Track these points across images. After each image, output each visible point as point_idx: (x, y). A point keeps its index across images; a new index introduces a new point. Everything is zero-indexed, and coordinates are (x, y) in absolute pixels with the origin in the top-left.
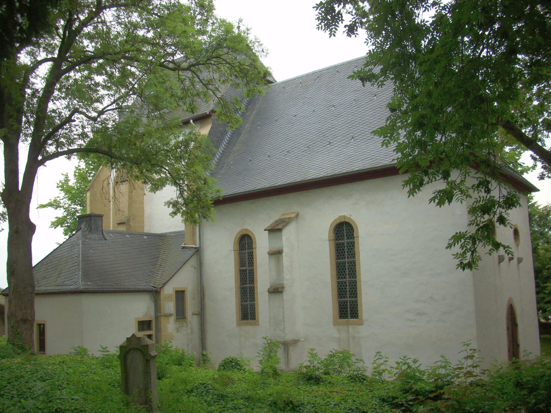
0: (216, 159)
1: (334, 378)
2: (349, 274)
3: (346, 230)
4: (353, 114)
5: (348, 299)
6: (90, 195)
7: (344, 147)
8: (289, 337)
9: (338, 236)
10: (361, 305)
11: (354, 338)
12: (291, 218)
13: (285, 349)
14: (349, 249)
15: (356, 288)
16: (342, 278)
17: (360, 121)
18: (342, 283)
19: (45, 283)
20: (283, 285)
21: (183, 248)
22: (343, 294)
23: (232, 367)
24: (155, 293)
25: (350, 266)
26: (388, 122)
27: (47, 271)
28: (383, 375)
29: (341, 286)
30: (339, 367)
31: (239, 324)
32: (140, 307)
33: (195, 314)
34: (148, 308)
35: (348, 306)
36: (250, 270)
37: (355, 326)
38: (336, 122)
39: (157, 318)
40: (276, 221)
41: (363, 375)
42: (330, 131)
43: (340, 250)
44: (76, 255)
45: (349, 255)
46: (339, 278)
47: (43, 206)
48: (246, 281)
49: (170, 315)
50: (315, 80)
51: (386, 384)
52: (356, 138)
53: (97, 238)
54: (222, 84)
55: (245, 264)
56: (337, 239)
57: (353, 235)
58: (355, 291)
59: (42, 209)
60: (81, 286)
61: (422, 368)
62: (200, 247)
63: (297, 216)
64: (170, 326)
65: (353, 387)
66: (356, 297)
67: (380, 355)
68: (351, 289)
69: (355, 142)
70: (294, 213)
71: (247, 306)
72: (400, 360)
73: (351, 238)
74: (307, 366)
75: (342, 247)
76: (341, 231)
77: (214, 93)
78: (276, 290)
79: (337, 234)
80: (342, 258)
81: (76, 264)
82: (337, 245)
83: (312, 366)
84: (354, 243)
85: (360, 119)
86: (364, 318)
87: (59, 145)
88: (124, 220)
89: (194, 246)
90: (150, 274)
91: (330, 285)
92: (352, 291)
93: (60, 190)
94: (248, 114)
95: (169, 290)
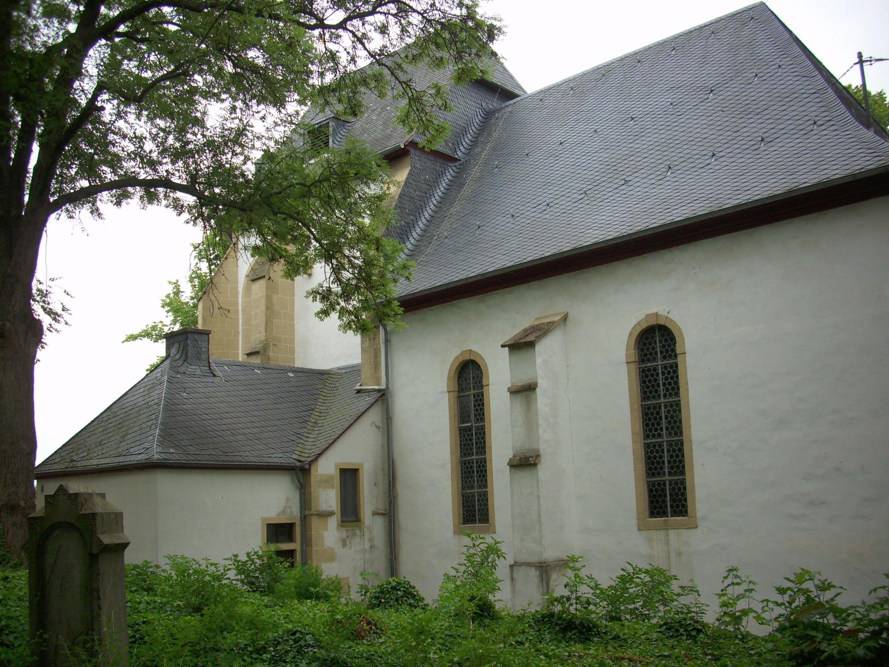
0: (418, 231)
1: (628, 627)
2: (667, 429)
3: (661, 341)
4: (669, 128)
5: (667, 478)
6: (203, 307)
7: (654, 186)
8: (550, 554)
9: (645, 355)
10: (693, 488)
11: (679, 554)
12: (553, 322)
13: (541, 577)
14: (666, 378)
15: (683, 456)
16: (654, 436)
17: (684, 138)
18: (654, 446)
19: (100, 453)
20: (538, 450)
21: (359, 391)
22: (656, 469)
23: (397, 600)
24: (300, 472)
25: (669, 412)
27: (105, 432)
28: (744, 623)
29: (652, 452)
30: (643, 606)
31: (458, 532)
32: (273, 498)
33: (378, 514)
34: (288, 500)
35: (666, 491)
36: (477, 428)
38: (638, 146)
39: (304, 518)
40: (525, 330)
41: (697, 622)
42: (626, 162)
43: (650, 381)
44: (156, 401)
45: (667, 390)
46: (647, 437)
47: (133, 338)
48: (471, 449)
49: (330, 514)
50: (597, 80)
51: (751, 644)
53: (198, 372)
54: (411, 63)
55: (469, 416)
56: (643, 361)
57: (673, 350)
58: (682, 461)
59: (132, 342)
60: (156, 454)
61: (842, 602)
62: (387, 388)
63: (565, 318)
64: (329, 534)
65: (673, 647)
66: (683, 473)
67: (736, 576)
68: (671, 456)
69: (674, 175)
70: (557, 314)
71: (473, 496)
72: (786, 584)
73: (670, 357)
74: (563, 597)
75: (652, 375)
76: (650, 344)
77: (392, 73)
78: (525, 462)
79: (642, 350)
80: (654, 397)
81: (154, 417)
82: (643, 371)
83: (574, 596)
84: (677, 366)
85: (682, 134)
86: (699, 514)
87: (89, 169)
88: (258, 347)
89: (376, 387)
90: (294, 438)
92: (675, 461)
93: (168, 312)
94: (478, 150)
95: (327, 467)
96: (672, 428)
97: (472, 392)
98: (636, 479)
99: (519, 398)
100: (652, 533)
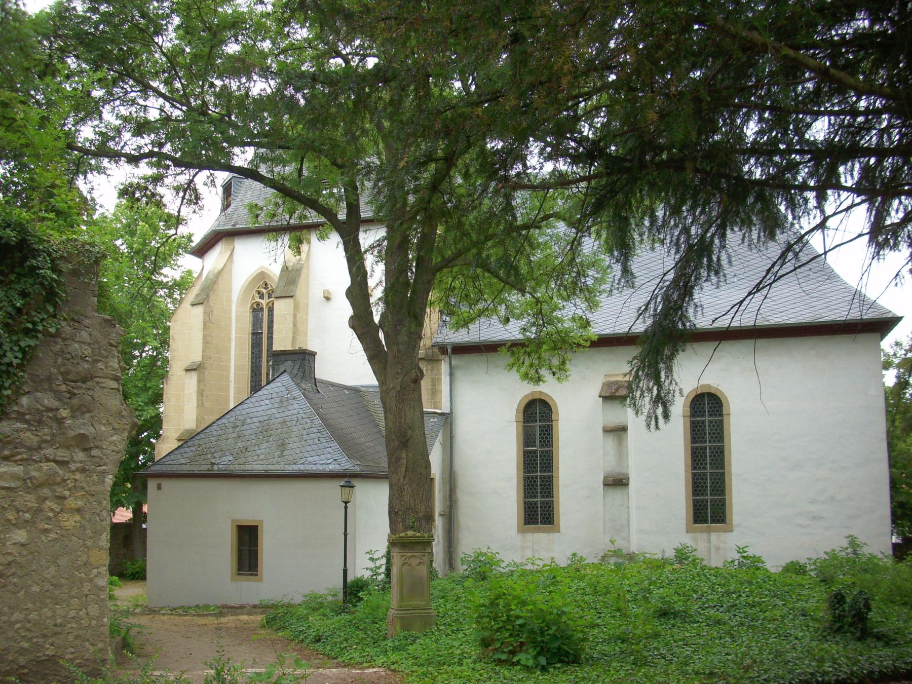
11: (718, 549)
20: (627, 475)
26: (616, 253)
31: (521, 531)
37: (721, 534)
52: (741, 276)
55: (535, 442)
57: (721, 411)
68: (713, 483)
86: (734, 523)
91: (683, 478)
96: (715, 464)
97: (538, 423)
98: (686, 497)
99: (611, 435)
100: (698, 535)
